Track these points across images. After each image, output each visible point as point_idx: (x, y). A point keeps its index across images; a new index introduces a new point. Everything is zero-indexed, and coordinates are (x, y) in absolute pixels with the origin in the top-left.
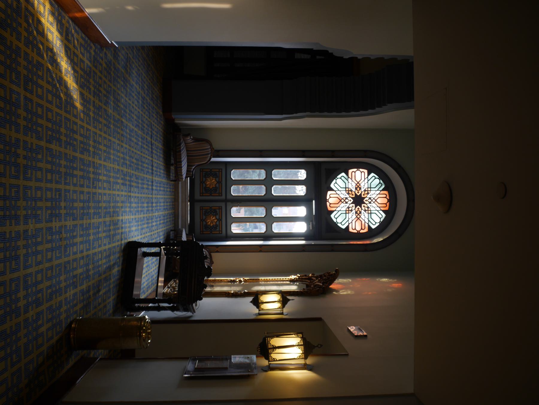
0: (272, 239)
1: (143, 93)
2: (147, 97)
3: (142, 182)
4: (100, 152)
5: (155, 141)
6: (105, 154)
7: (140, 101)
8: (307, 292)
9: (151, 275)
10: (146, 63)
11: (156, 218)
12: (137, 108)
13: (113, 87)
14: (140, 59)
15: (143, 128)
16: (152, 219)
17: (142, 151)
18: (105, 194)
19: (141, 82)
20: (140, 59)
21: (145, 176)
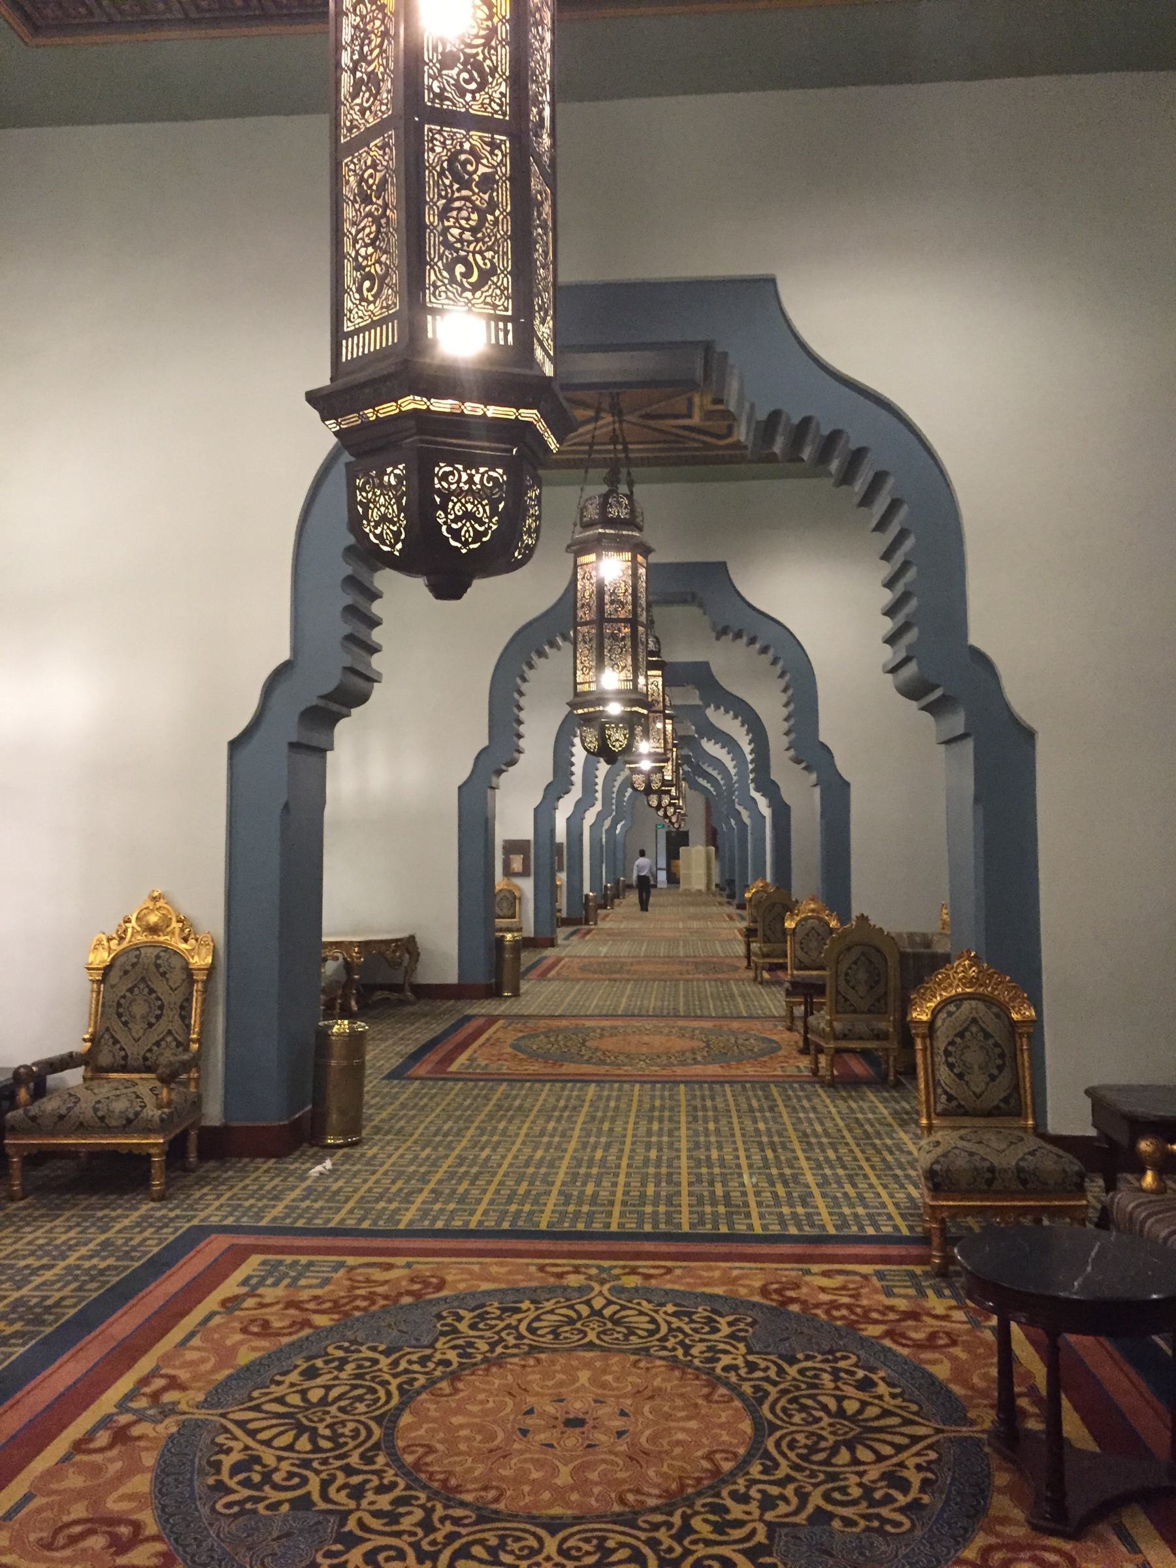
0: (105, 1075)
1: (392, 1107)
2: (304, 1190)
3: (585, 1164)
4: (534, 1193)
5: (489, 1100)
6: (538, 1183)
7: (355, 1168)
8: (332, 1017)
9: (879, 1214)
10: (214, 1175)
11: (694, 1097)
12: (374, 1178)
13: (386, 1167)
14: (198, 1194)
15: (385, 1217)
16: (695, 1108)
17: (331, 1461)
18: (627, 1184)
19: (259, 1200)
20: (198, 1194)
21: (579, 1126)
